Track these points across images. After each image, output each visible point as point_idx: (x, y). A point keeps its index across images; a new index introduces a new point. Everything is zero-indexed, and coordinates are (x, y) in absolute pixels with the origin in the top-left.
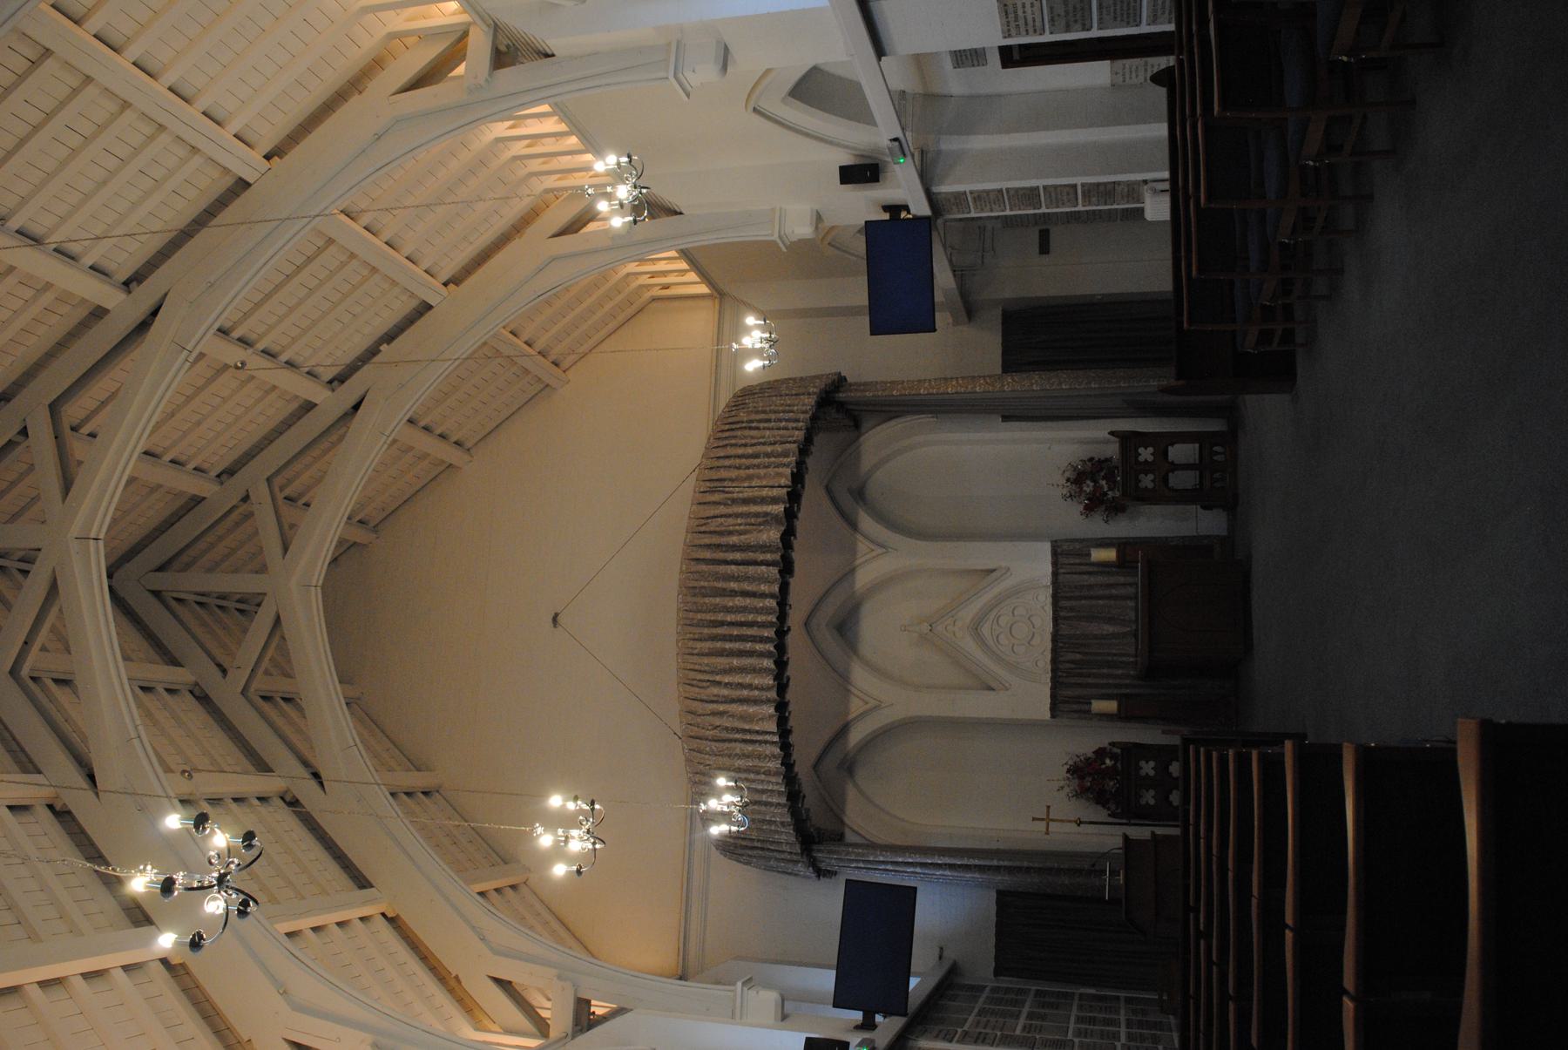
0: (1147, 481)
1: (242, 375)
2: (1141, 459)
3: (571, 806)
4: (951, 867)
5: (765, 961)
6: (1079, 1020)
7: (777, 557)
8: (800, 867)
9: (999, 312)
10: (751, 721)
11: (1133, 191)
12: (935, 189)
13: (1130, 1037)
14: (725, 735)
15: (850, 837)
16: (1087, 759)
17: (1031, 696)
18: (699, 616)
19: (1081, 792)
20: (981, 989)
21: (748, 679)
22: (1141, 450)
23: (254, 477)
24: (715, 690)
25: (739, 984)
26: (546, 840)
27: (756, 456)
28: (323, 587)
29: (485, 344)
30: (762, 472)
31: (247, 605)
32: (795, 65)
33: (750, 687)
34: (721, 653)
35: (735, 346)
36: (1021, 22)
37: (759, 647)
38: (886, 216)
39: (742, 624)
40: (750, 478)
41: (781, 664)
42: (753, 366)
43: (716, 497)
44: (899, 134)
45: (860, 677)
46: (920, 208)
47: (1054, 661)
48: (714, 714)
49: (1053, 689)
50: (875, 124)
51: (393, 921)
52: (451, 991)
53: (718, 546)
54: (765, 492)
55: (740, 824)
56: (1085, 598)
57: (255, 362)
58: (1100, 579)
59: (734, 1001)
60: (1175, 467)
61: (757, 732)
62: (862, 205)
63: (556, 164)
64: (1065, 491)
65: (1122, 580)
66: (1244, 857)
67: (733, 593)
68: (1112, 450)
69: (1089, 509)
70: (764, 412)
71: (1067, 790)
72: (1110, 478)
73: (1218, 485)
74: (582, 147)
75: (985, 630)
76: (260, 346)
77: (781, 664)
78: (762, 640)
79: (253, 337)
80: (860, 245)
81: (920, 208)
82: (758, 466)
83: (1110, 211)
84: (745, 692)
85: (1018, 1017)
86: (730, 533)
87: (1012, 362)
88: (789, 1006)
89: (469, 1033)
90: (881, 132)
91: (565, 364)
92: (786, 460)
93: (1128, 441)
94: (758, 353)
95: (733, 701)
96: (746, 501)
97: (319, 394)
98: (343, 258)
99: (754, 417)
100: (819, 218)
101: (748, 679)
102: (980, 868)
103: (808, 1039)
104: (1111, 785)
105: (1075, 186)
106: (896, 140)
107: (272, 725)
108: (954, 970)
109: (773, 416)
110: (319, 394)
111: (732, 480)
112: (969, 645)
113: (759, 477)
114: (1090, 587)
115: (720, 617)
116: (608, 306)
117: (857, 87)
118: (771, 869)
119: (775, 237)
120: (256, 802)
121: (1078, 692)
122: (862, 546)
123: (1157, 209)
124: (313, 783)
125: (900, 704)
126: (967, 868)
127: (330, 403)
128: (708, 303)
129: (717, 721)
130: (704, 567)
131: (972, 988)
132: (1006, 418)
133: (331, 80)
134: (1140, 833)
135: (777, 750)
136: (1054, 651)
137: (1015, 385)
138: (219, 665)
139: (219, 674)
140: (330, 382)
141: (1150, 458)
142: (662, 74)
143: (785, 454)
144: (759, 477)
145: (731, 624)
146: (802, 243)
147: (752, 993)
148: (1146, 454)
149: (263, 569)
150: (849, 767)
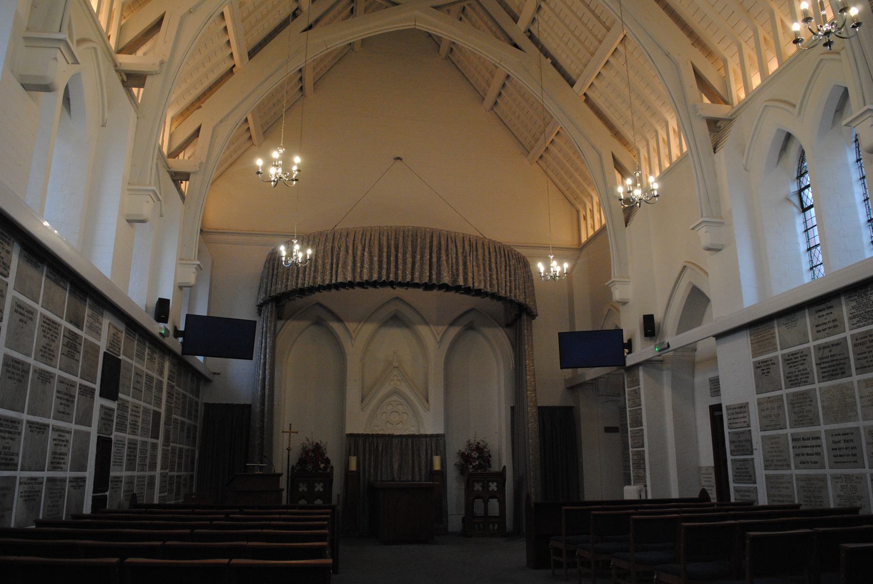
0: (478, 487)
2: (490, 484)
3: (295, 168)
5: (211, 277)
7: (434, 281)
8: (263, 296)
10: (343, 268)
12: (641, 368)
13: (171, 477)
14: (335, 253)
15: (280, 323)
16: (324, 454)
17: (358, 423)
18: (401, 238)
20: (198, 396)
21: (366, 266)
22: (495, 484)
24: (360, 248)
25: (198, 263)
26: (275, 154)
27: (490, 270)
28: (415, 29)
30: (482, 272)
32: (710, 289)
33: (362, 267)
34: (380, 250)
35: (552, 257)
36: (735, 416)
37: (384, 272)
38: (625, 341)
40: (478, 266)
42: (541, 267)
44: (671, 349)
45: (368, 328)
46: (630, 360)
47: (378, 436)
49: (363, 435)
50: (678, 333)
51: (231, 71)
52: (193, 104)
54: (470, 274)
55: (286, 261)
59: (190, 260)
61: (337, 271)
63: (654, 155)
65: (423, 472)
67: (414, 257)
68: (495, 468)
69: (462, 455)
72: (480, 466)
73: (476, 526)
74: (663, 169)
75: (395, 397)
81: (630, 360)
82: (484, 270)
86: (447, 255)
87: (546, 413)
89: (170, 114)
90: (674, 339)
91: (540, 162)
93: (500, 476)
95: (354, 257)
96: (465, 264)
97: (522, 24)
98: (591, 49)
100: (624, 303)
101: (366, 266)
102: (263, 395)
105: (643, 446)
106: (669, 346)
108: (207, 381)
109: (512, 279)
110: (522, 24)
111: (477, 255)
112: (387, 388)
113: (479, 271)
115: (401, 250)
117: (699, 323)
118: (262, 279)
119: (613, 279)
122: (441, 329)
123: (630, 492)
124: (306, 26)
125: (353, 350)
127: (518, 31)
128: (576, 242)
129: (343, 249)
130: (428, 241)
131: (198, 391)
132: (512, 408)
135: (327, 282)
136: (383, 436)
137: (531, 411)
140: (529, 31)
141: (490, 489)
142: (704, 215)
143: (491, 285)
144: (479, 271)
145: (397, 256)
146: (608, 293)
147: (194, 270)
148: (493, 486)
150: (319, 322)
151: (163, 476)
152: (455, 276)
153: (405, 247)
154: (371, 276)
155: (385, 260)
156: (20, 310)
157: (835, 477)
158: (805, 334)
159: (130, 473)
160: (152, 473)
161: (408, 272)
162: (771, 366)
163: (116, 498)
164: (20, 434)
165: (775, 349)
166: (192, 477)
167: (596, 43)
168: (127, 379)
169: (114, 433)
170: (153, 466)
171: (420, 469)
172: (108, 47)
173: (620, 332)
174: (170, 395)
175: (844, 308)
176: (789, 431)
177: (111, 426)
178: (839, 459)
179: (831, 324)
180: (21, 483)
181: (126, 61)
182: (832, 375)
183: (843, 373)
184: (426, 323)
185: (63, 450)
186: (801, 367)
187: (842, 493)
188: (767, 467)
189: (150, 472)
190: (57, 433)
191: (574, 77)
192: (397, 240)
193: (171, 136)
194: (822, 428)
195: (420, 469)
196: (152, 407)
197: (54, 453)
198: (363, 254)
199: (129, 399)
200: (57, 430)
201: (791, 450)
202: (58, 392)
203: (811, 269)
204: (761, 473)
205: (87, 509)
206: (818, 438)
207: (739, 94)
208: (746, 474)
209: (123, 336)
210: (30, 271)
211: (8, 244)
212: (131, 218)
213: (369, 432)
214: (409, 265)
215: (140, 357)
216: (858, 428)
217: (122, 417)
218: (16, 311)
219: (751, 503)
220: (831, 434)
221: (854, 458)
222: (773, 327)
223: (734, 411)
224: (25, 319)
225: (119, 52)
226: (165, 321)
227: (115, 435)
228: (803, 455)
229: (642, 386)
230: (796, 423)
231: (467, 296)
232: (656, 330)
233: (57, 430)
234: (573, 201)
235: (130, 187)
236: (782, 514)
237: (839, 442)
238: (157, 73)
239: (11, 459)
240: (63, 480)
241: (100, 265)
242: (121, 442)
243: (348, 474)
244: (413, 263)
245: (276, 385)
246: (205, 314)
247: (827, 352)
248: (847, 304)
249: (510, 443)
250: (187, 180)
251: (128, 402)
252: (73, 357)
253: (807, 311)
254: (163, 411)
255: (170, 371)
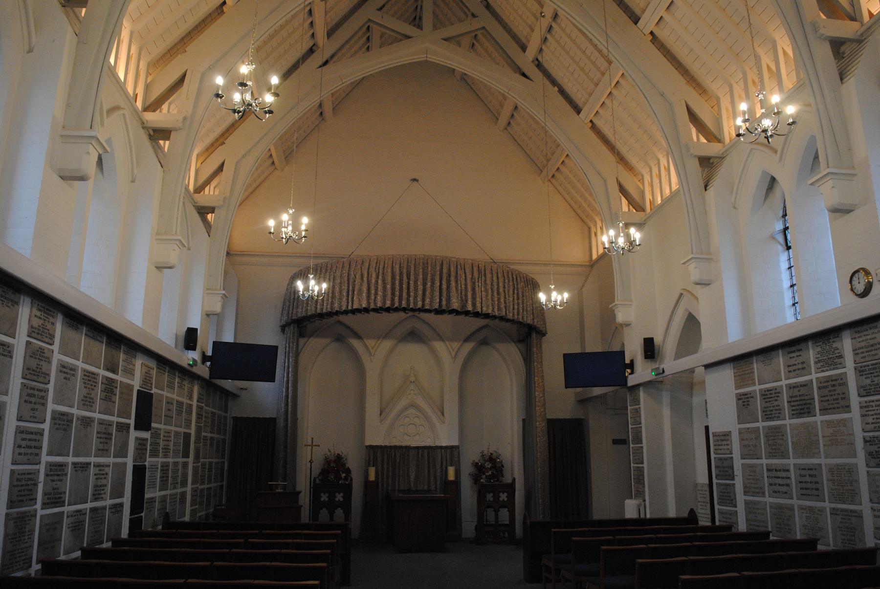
0: (490, 497)
1: (538, 15)
2: (501, 494)
3: (303, 227)
4: (287, 396)
5: (238, 302)
6: (211, 463)
7: (444, 307)
8: (285, 318)
9: (580, 416)
10: (358, 295)
11: (640, 494)
12: (641, 388)
13: (202, 490)
14: (351, 281)
15: (302, 341)
16: (345, 464)
18: (413, 267)
19: (327, 461)
20: (226, 412)
21: (380, 293)
22: (506, 494)
23: (485, 20)
24: (374, 276)
26: (285, 217)
27: (498, 294)
28: (426, 61)
29: (558, 146)
30: (489, 297)
31: (417, 21)
32: (703, 317)
33: (376, 294)
34: (393, 278)
35: (553, 287)
36: (720, 443)
38: (627, 361)
39: (408, 289)
40: (486, 291)
41: (388, 310)
42: (542, 297)
43: (476, 274)
44: (666, 374)
45: (387, 344)
46: (632, 381)
47: (396, 447)
48: (362, 275)
49: (381, 447)
50: (675, 359)
52: (217, 140)
53: (450, 276)
54: (478, 300)
55: (303, 295)
56: (429, 464)
57: (545, 23)
58: (438, 474)
59: (216, 290)
60: (496, 512)
61: (353, 298)
62: (633, 349)
63: (656, 181)
64: (486, 452)
66: (299, 546)
67: (425, 284)
68: (507, 479)
69: (476, 465)
70: (523, 296)
71: (329, 453)
72: (493, 476)
73: (490, 534)
74: (664, 197)
75: (412, 411)
76: (554, 25)
77: (388, 310)
78: (400, 300)
79: (559, 21)
80: (616, 348)
81: (632, 381)
82: (493, 295)
83: (633, 483)
84: (373, 292)
85: (211, 432)
86: (456, 282)
87: (554, 425)
88: (215, 318)
89: (196, 152)
90: (671, 365)
91: (553, 181)
92: (496, 310)
94: (549, 300)
95: (369, 285)
96: (473, 289)
98: (595, 80)
99: (520, 291)
100: (628, 325)
102: (286, 411)
103: (196, 330)
104: (332, 477)
105: (642, 463)
106: (663, 371)
107: (357, 32)
108: (235, 396)
109: (520, 301)
112: (403, 403)
113: (487, 296)
114: (434, 465)
115: (412, 278)
116: (585, 205)
117: (696, 351)
118: (285, 300)
119: (616, 302)
120: (311, 33)
121: (379, 459)
122: (456, 345)
123: (630, 509)
124: (320, 63)
125: (372, 366)
126: (287, 405)
127: (526, 60)
128: (587, 259)
129: (358, 276)
130: (438, 268)
131: (226, 406)
132: (524, 420)
133: (694, 67)
134: (305, 500)
135: (344, 308)
136: (401, 447)
137: (540, 426)
138: (384, 6)
139: (379, 6)
140: (537, 59)
142: (694, 250)
144: (487, 296)
145: (409, 284)
146: (613, 317)
147: (220, 298)
148: (504, 497)
149: (435, 27)
150: (339, 339)
151: (194, 490)
152: (464, 302)
153: (416, 275)
154: (385, 303)
155: (397, 287)
156: (65, 370)
157: (801, 508)
158: (779, 373)
159: (163, 493)
160: (183, 490)
161: (419, 299)
162: (750, 400)
163: (151, 519)
164: (66, 475)
165: (754, 384)
166: (221, 487)
167: (599, 75)
168: (159, 409)
169: (148, 459)
170: (184, 483)
171: (435, 477)
172: (135, 109)
173: (622, 353)
174: (199, 416)
175: (811, 352)
176: (764, 461)
177: (145, 454)
178: (804, 492)
179: (800, 366)
180: (68, 517)
181: (151, 118)
182: (800, 413)
183: (809, 412)
184: (441, 339)
185: (104, 482)
186: (776, 403)
187: (806, 523)
188: (745, 493)
189: (183, 491)
190: (98, 469)
191: (580, 105)
192: (408, 267)
193: (197, 171)
194: (791, 462)
195: (435, 477)
196: (182, 430)
197: (96, 486)
198: (377, 282)
199: (162, 426)
200: (98, 466)
201: (766, 479)
202: (98, 433)
203: (794, 305)
204: (741, 498)
205: (125, 533)
206: (788, 471)
207: (729, 133)
208: (729, 498)
209: (154, 372)
210: (72, 334)
211: (53, 317)
212: (159, 265)
213: (387, 443)
214: (420, 292)
215: (171, 386)
216: (820, 465)
217: (155, 444)
218: (61, 371)
219: (729, 528)
220: (799, 468)
221: (816, 492)
222: (752, 363)
223: (719, 438)
224: (68, 376)
225: (146, 109)
226: (194, 348)
227: (149, 461)
228: (775, 484)
229: (642, 406)
230: (771, 455)
231: (476, 319)
232: (656, 351)
233: (98, 466)
234: (585, 218)
235: (160, 237)
236: (756, 539)
237: (805, 476)
238: (180, 129)
239: (60, 498)
240: (104, 508)
241: (132, 316)
242: (154, 467)
243: (367, 484)
244: (424, 291)
245: (299, 399)
246: (232, 341)
247: (796, 392)
248: (813, 349)
249: (522, 452)
250: (213, 212)
251: (160, 429)
252: (110, 400)
253: (780, 351)
254: (193, 431)
255: (199, 394)
